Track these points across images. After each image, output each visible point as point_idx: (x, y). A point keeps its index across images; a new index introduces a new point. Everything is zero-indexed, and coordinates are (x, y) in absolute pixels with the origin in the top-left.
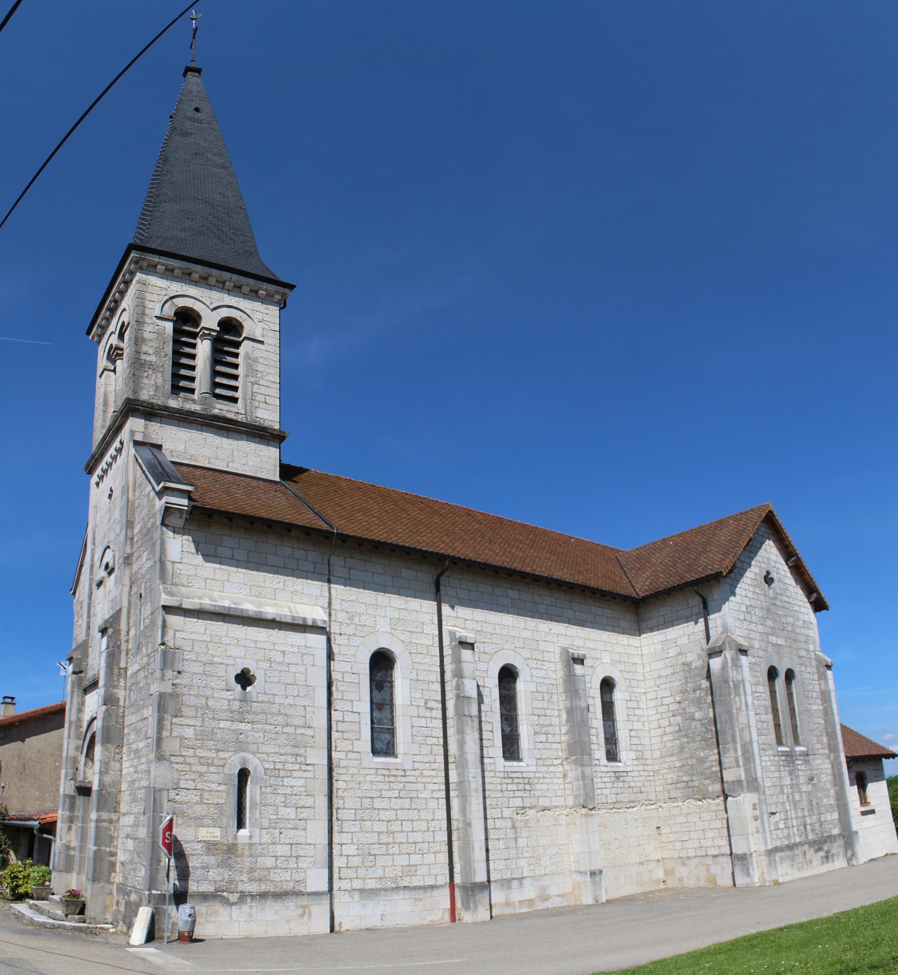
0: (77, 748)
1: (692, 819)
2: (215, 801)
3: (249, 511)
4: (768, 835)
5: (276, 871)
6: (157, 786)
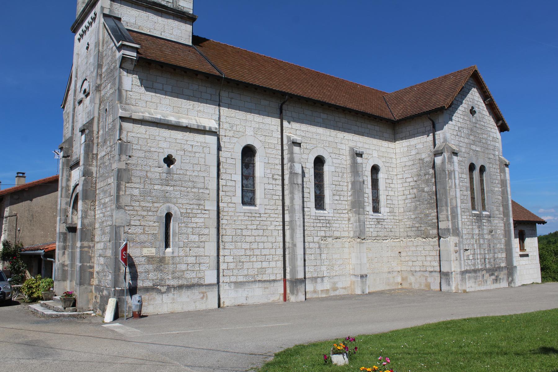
0: (67, 203)
1: (419, 249)
2: (152, 232)
3: (173, 62)
4: (462, 262)
5: (188, 272)
6: (117, 224)
